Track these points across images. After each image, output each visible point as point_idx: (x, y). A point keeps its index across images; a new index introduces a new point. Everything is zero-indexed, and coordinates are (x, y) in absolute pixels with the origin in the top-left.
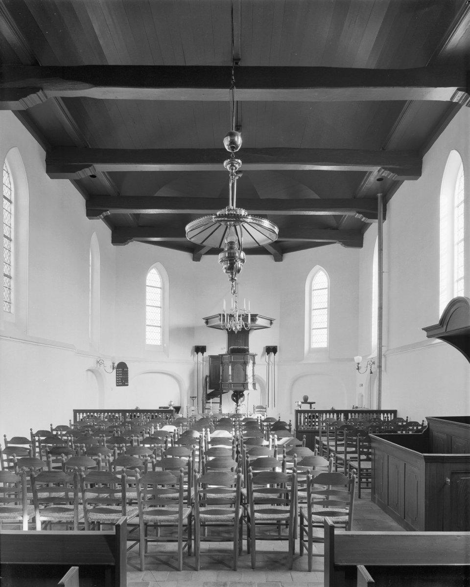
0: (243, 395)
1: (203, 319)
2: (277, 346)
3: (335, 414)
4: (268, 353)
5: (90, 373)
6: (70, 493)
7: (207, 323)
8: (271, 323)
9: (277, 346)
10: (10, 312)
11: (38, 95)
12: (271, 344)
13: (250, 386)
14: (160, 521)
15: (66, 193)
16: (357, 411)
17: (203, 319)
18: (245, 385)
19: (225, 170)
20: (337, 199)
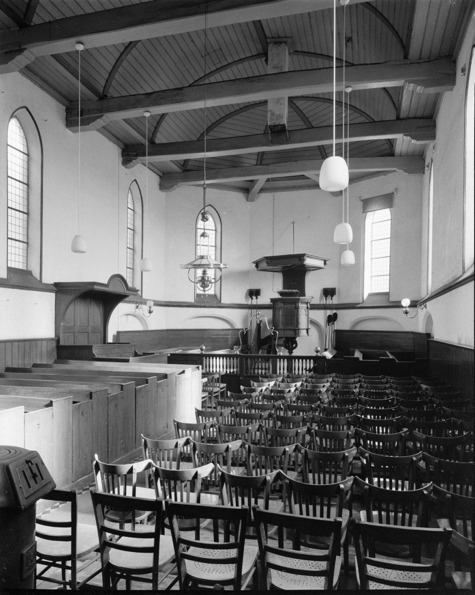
0: (296, 343)
1: (253, 263)
2: (335, 288)
3: (286, 360)
4: (326, 297)
5: (130, 317)
6: (381, 473)
7: (257, 266)
8: (325, 263)
9: (335, 288)
10: (372, 259)
11: (315, 48)
12: (329, 286)
13: (303, 332)
14: (103, 483)
15: (95, 145)
16: (231, 355)
17: (253, 263)
18: (296, 331)
19: (70, 128)
20: (397, 141)
